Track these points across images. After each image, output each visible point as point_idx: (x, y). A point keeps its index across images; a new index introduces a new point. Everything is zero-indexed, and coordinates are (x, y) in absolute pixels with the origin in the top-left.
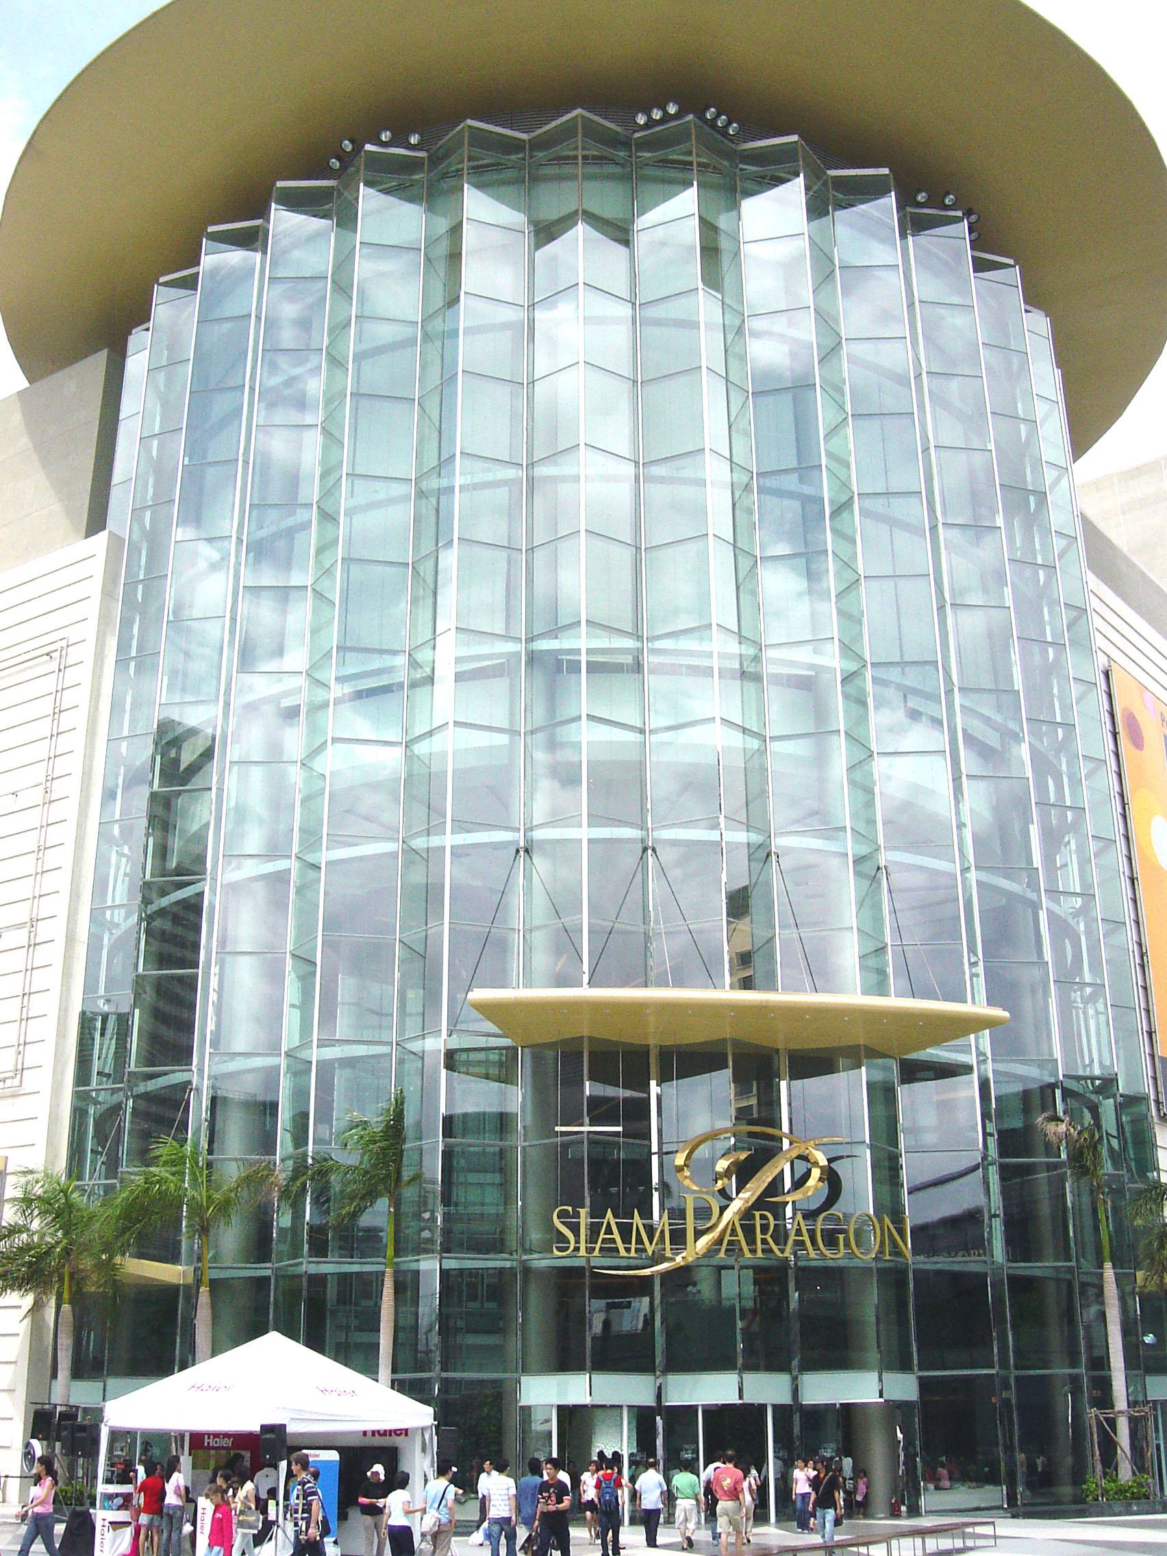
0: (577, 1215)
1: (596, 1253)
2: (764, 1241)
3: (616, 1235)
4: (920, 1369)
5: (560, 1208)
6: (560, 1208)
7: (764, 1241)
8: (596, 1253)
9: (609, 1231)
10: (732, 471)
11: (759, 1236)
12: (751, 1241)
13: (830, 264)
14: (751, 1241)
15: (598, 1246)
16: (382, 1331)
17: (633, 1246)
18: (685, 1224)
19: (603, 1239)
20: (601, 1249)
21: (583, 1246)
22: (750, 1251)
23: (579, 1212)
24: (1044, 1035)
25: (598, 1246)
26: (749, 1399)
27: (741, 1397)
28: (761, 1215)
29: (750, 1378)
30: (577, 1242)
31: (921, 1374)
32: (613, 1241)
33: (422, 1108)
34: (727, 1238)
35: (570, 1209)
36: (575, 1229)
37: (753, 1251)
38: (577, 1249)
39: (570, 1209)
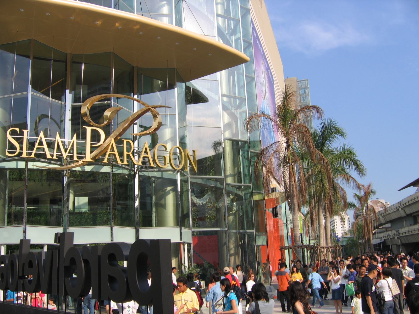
0: (22, 134)
1: (33, 156)
2: (128, 156)
3: (45, 146)
4: (194, 227)
5: (11, 129)
6: (11, 129)
7: (128, 156)
8: (33, 156)
9: (41, 143)
10: (344, 138)
11: (126, 153)
12: (121, 154)
13: (401, 239)
14: (121, 154)
15: (34, 152)
16: (330, 235)
17: (55, 153)
18: (91, 144)
19: (37, 148)
20: (36, 155)
21: (25, 151)
22: (121, 160)
23: (23, 132)
24: (259, 45)
25: (34, 152)
26: (116, 240)
27: (181, 239)
28: (127, 142)
29: (117, 229)
30: (21, 148)
31: (193, 230)
32: (43, 150)
33: (160, 150)
34: (109, 152)
35: (18, 129)
36: (20, 141)
37: (122, 161)
38: (21, 154)
39: (18, 129)
